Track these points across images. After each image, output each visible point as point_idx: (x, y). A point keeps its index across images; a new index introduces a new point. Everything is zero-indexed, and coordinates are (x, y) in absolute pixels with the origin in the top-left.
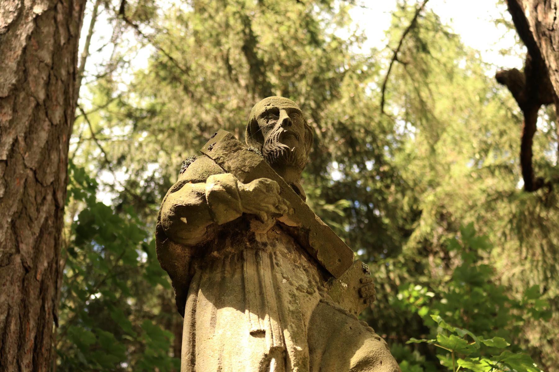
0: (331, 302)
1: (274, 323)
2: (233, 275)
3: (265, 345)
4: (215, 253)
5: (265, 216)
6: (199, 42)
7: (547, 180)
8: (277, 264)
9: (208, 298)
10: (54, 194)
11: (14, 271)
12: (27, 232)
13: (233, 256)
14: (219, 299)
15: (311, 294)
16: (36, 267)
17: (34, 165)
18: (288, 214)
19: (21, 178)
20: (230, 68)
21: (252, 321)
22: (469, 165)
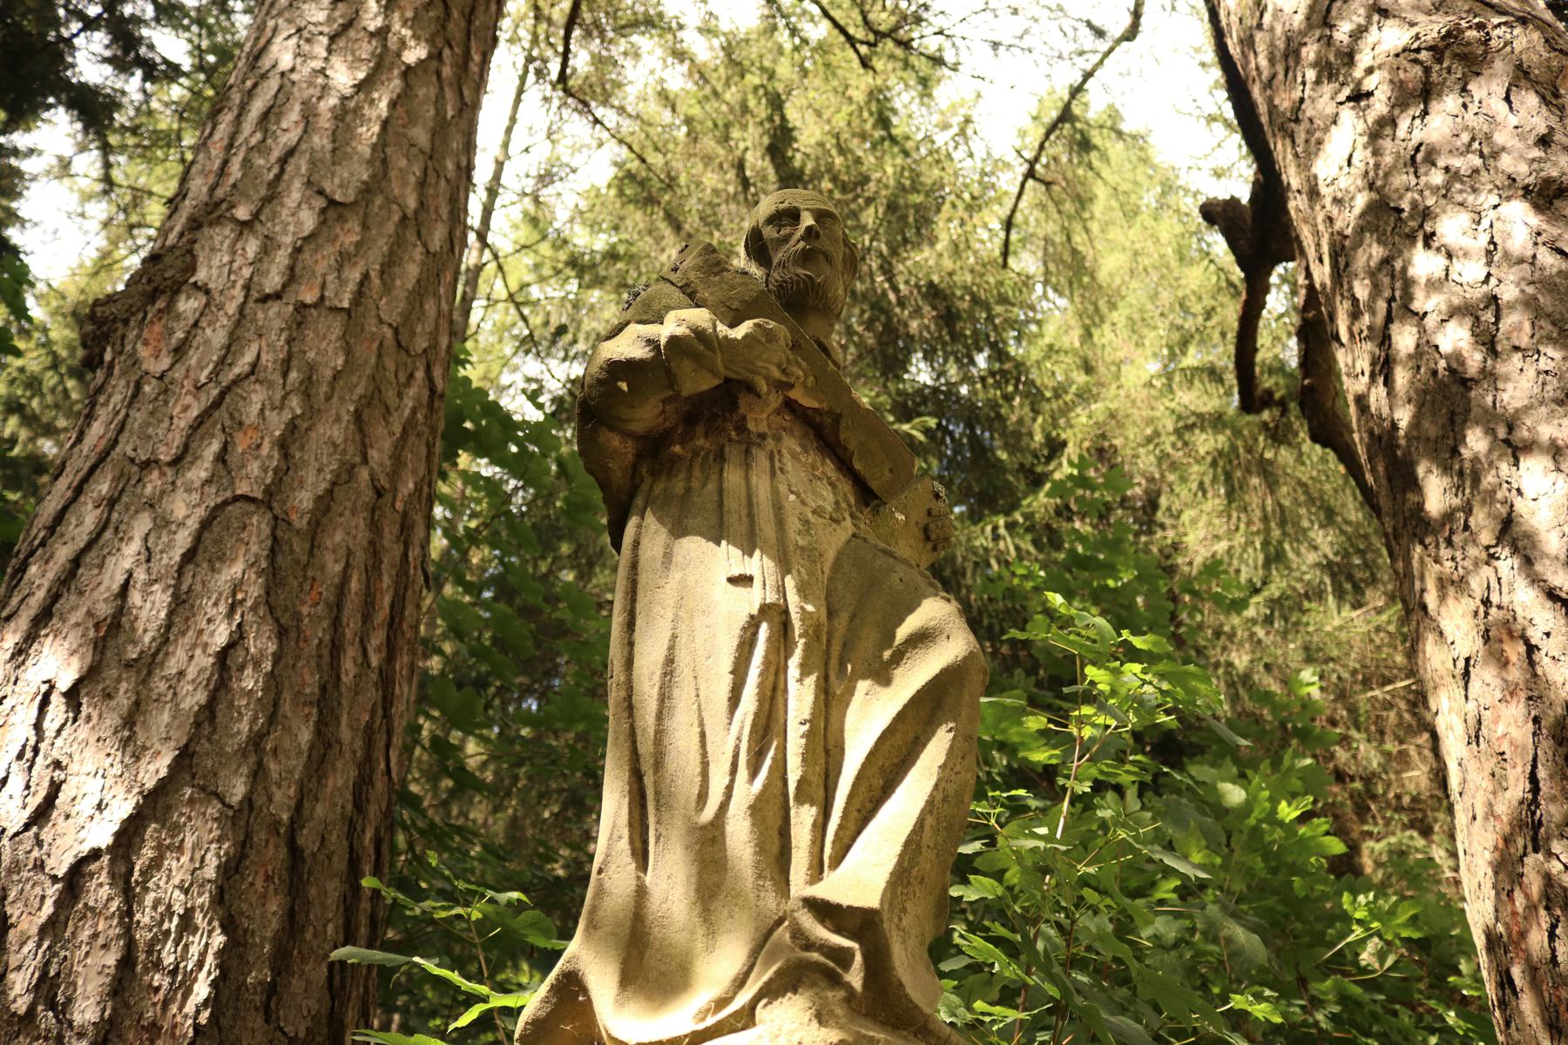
0: (872, 539)
1: (769, 564)
2: (704, 485)
3: (751, 600)
4: (677, 449)
5: (763, 387)
6: (693, 137)
7: (1277, 396)
8: (782, 470)
9: (660, 520)
10: (428, 370)
11: (359, 493)
12: (381, 430)
13: (707, 454)
14: (680, 523)
15: (837, 521)
16: (395, 489)
17: (394, 319)
18: (804, 385)
19: (374, 340)
20: (745, 183)
21: (732, 560)
22: (1154, 367)
